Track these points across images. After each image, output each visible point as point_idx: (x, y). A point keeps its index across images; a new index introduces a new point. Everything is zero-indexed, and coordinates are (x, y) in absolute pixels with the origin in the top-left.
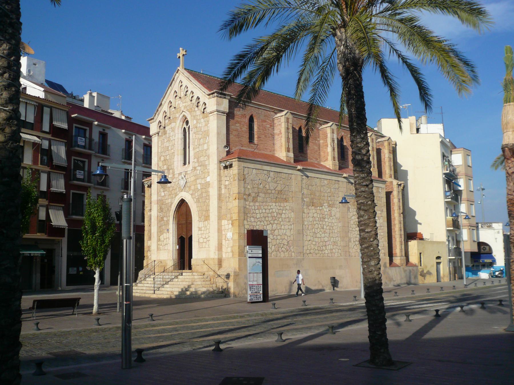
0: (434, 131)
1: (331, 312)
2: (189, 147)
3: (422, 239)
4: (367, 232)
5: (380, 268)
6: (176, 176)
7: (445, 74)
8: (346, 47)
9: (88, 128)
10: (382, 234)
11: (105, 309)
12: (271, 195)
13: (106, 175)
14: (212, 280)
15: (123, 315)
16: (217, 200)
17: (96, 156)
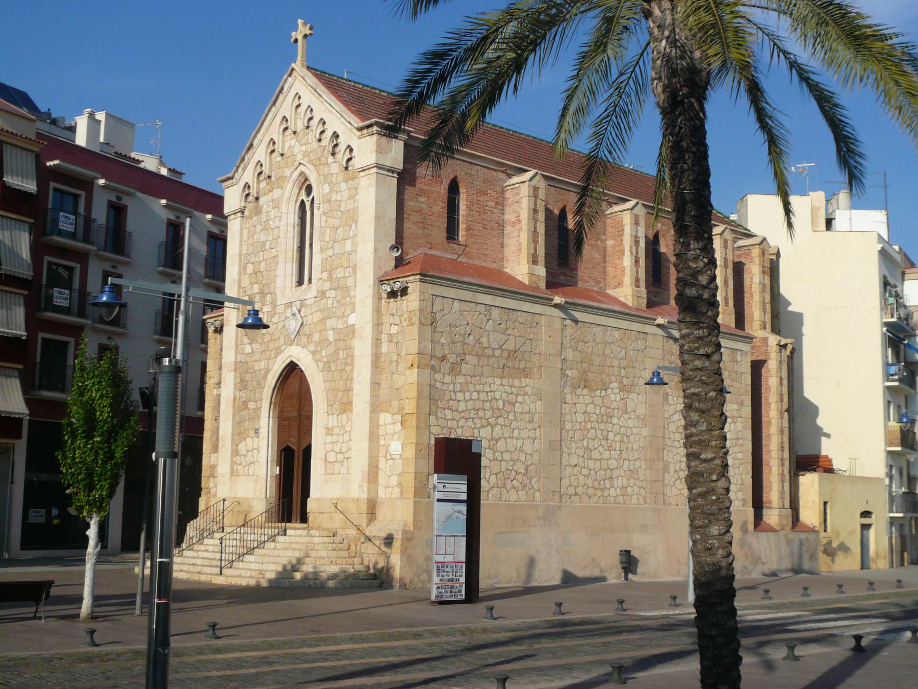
0: (865, 227)
1: (619, 631)
2: (311, 245)
3: (830, 470)
4: (705, 461)
5: (730, 543)
6: (280, 309)
7: (893, 110)
8: (673, 42)
9: (83, 194)
10: (739, 456)
11: (107, 609)
12: (493, 360)
13: (123, 306)
14: (353, 548)
15: (150, 629)
16: (369, 368)
17: (99, 257)
